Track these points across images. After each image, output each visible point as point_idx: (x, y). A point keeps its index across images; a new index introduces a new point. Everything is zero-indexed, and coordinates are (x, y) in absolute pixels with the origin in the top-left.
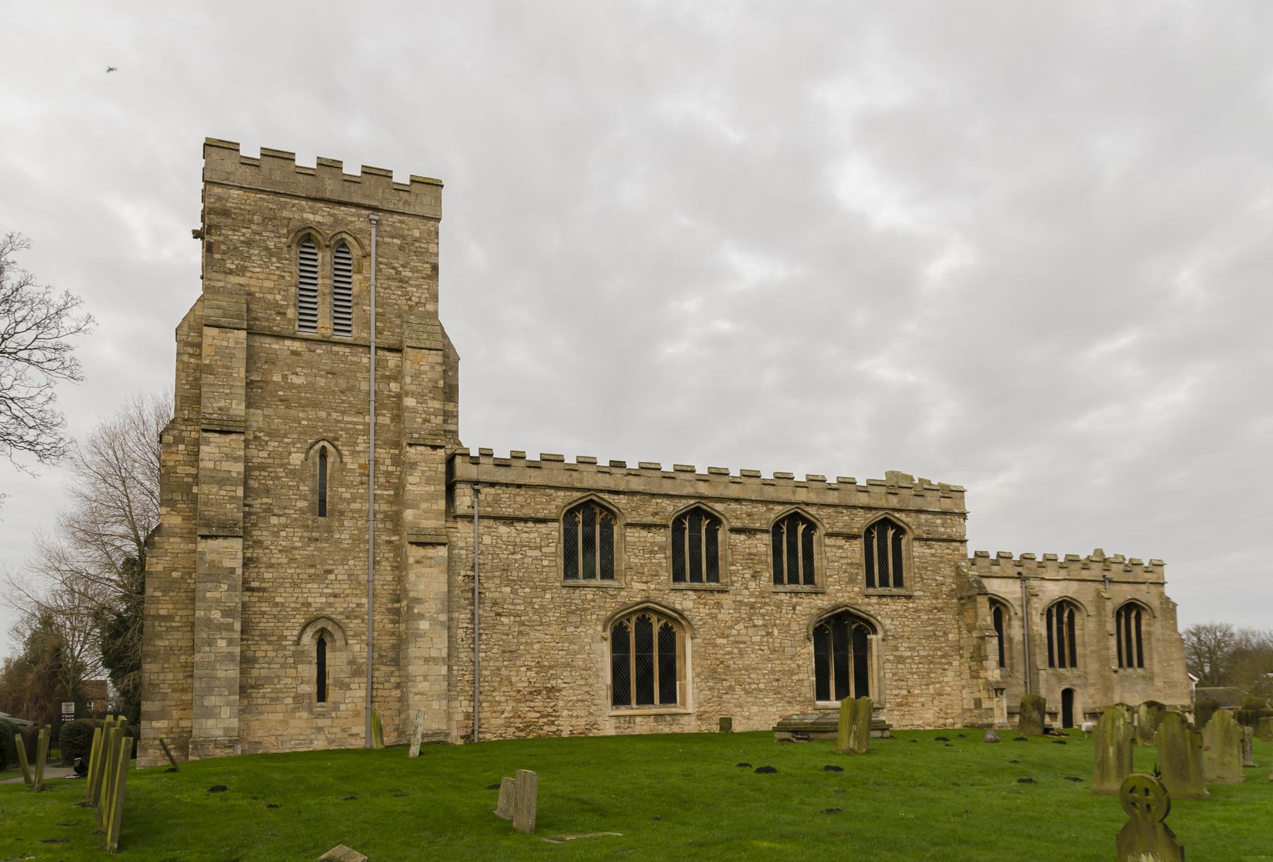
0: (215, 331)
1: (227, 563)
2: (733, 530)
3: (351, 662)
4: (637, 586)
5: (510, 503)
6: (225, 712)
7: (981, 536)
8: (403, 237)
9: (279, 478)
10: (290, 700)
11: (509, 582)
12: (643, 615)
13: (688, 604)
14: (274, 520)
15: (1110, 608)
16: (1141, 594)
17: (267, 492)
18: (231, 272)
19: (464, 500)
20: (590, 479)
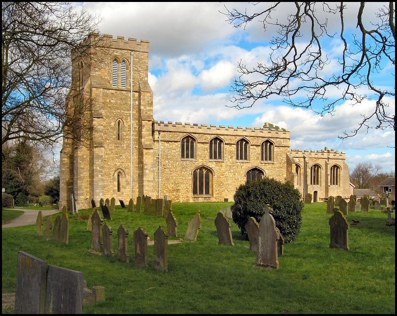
3: (126, 181)
4: (200, 160)
5: (168, 136)
8: (139, 58)
9: (108, 129)
10: (112, 191)
11: (168, 159)
12: (202, 168)
13: (213, 166)
14: (107, 141)
15: (329, 167)
18: (97, 71)
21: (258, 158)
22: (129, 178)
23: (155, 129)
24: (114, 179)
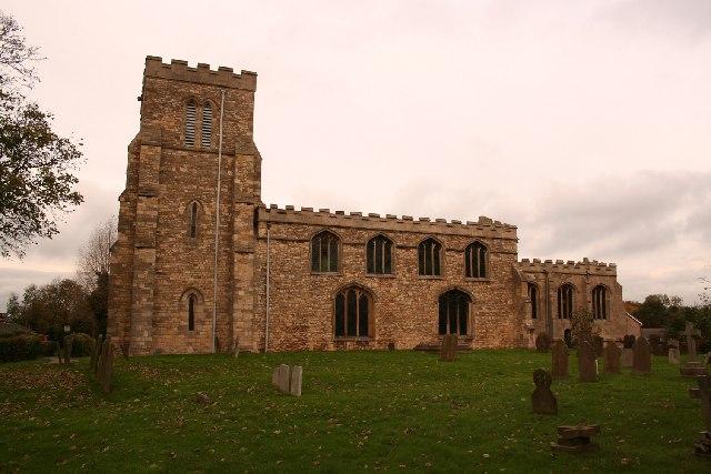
0: (146, 147)
1: (148, 261)
2: (399, 247)
3: (205, 311)
4: (349, 275)
5: (284, 232)
6: (146, 334)
7: (526, 251)
12: (354, 287)
13: (375, 285)
15: (589, 288)
16: (606, 282)
17: (168, 226)
19: (262, 232)
20: (326, 221)
21: (459, 272)
22: (210, 304)
23: (261, 217)
24: (181, 308)
